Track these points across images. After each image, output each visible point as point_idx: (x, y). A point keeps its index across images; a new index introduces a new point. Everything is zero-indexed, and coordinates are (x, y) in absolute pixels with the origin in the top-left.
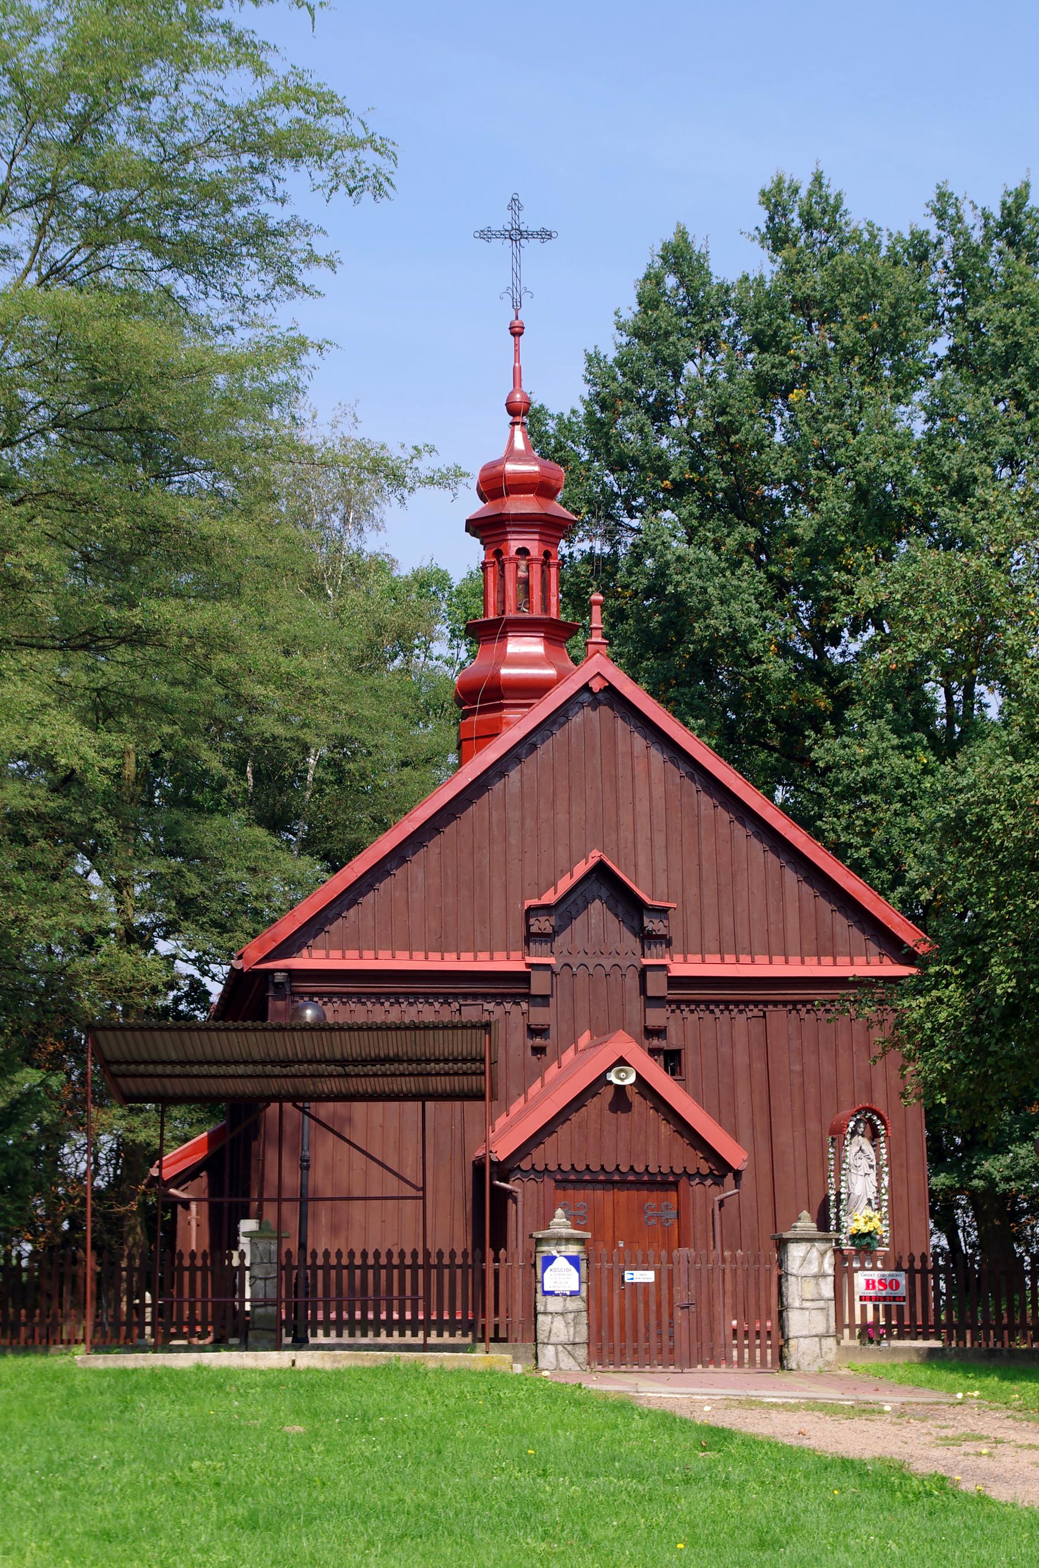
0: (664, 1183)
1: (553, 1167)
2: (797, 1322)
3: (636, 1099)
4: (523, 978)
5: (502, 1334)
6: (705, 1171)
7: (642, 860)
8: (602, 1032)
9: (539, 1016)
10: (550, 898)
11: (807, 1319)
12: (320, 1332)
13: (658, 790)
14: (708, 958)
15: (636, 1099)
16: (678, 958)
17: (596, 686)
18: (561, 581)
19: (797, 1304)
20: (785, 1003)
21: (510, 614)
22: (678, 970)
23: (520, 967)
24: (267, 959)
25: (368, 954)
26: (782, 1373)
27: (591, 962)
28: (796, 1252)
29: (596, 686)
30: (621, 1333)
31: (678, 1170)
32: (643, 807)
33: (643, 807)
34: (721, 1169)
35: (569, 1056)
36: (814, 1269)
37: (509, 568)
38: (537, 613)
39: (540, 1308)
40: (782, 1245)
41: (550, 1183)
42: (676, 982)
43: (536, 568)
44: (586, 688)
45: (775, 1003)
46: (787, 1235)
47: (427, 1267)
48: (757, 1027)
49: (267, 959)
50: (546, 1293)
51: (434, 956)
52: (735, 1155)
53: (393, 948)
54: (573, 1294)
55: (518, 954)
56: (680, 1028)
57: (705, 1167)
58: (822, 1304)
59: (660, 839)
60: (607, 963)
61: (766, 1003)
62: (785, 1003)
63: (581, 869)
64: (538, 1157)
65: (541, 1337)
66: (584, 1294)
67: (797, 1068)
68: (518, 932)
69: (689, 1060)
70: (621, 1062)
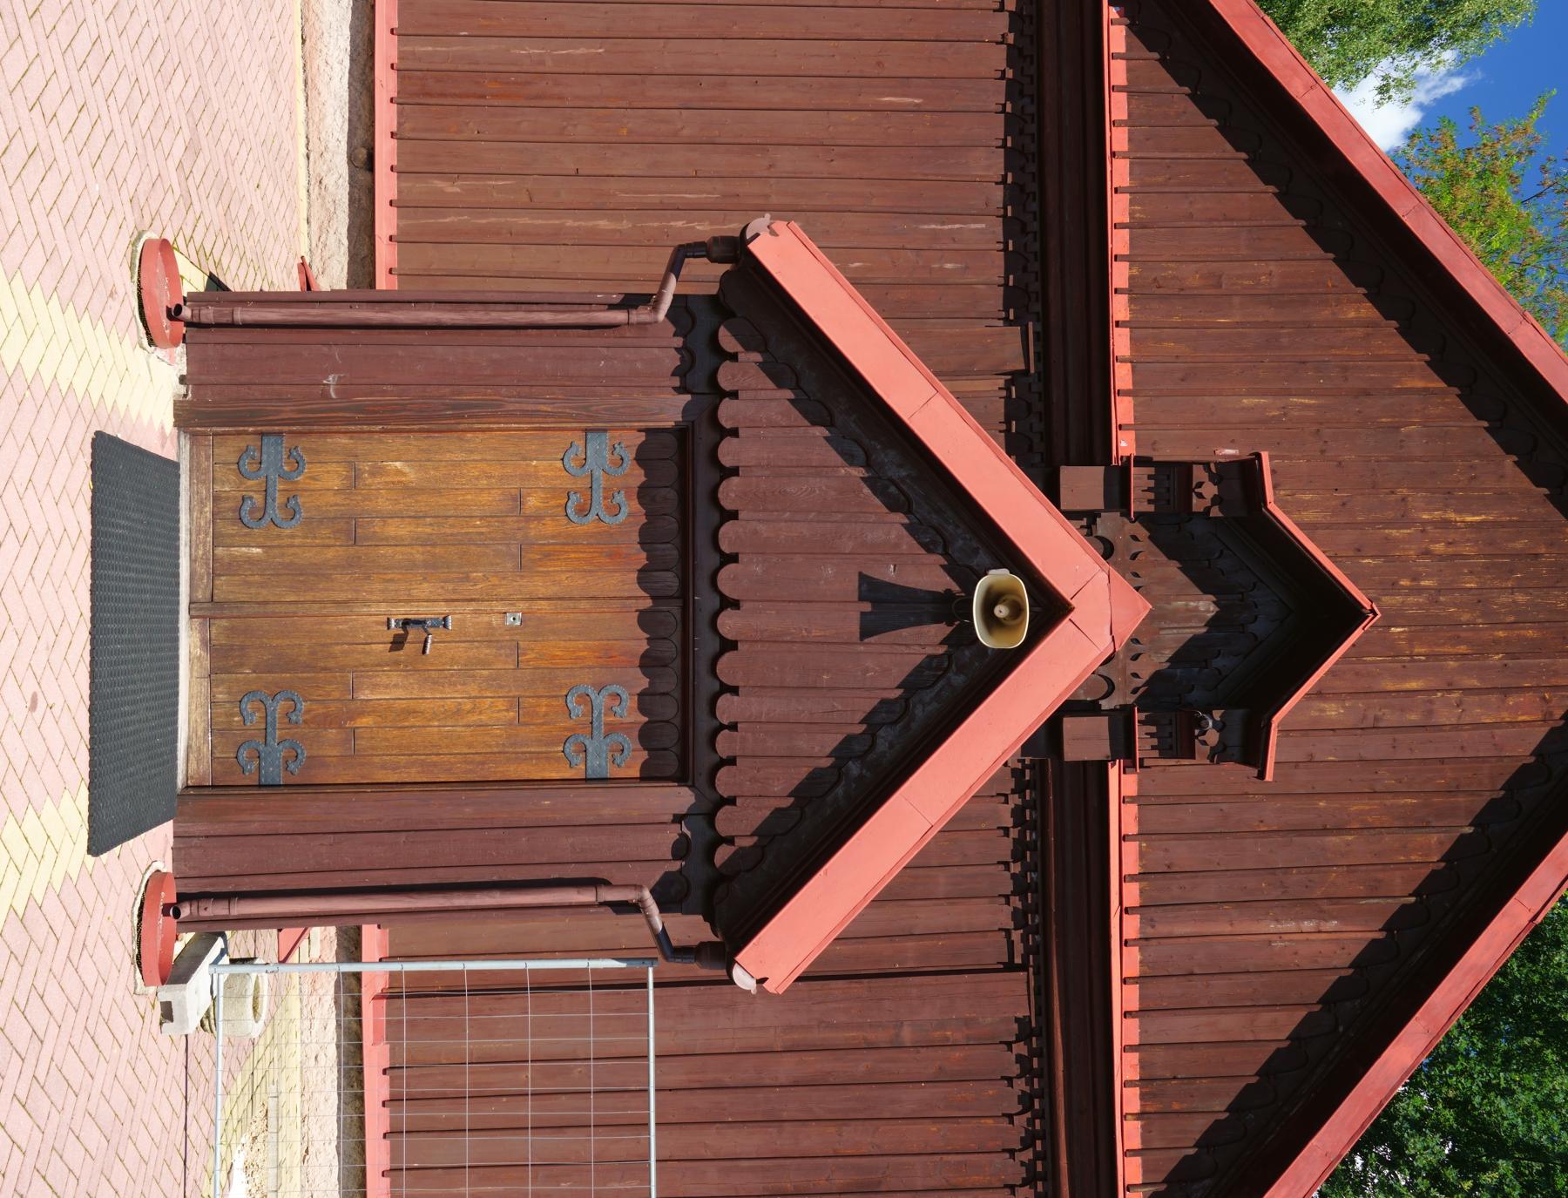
0: (681, 738)
6: (726, 821)
31: (726, 782)
34: (734, 892)
41: (670, 408)
45: (1042, 993)
48: (995, 951)
52: (778, 954)
62: (1044, 1010)
67: (907, 1035)
70: (1050, 608)
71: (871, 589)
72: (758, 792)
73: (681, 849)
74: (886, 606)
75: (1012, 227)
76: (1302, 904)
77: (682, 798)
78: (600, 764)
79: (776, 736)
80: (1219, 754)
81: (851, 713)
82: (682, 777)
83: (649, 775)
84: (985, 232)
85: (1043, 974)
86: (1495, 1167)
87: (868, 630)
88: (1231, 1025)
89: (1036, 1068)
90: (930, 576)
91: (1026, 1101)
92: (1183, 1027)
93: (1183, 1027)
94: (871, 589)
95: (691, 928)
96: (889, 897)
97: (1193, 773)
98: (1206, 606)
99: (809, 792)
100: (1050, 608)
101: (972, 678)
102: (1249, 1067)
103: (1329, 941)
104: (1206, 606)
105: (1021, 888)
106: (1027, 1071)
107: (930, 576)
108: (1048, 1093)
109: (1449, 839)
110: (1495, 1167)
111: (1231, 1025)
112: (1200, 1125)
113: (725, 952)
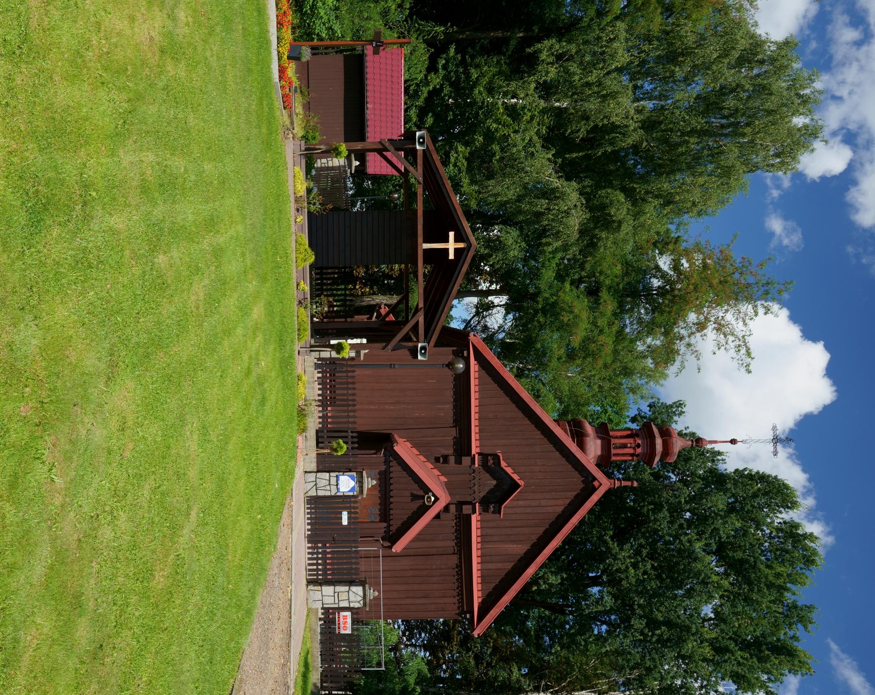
0: (385, 515)
1: (391, 469)
2: (328, 590)
3: (418, 503)
4: (469, 453)
5: (321, 445)
6: (391, 528)
7: (521, 503)
8: (449, 487)
9: (452, 459)
10: (503, 464)
11: (328, 595)
12: (320, 375)
13: (550, 509)
14: (479, 531)
15: (418, 503)
16: (479, 518)
17: (596, 483)
18: (626, 461)
19: (334, 488)
20: (460, 562)
21: (613, 441)
22: (474, 518)
23: (473, 452)
24: (474, 346)
25: (477, 389)
26: (305, 582)
27: (476, 481)
28: (359, 590)
29: (596, 483)
30: (322, 509)
31: (391, 522)
32: (543, 503)
33: (543, 503)
34: (392, 538)
35: (436, 472)
36: (352, 598)
37: (631, 440)
38: (613, 451)
39: (332, 474)
40: (362, 584)
41: (383, 468)
42: (468, 518)
43: (631, 451)
44: (595, 479)
45: (460, 558)
46: (367, 586)
47: (321, 279)
48: (451, 550)
49: (474, 346)
50: (337, 477)
51: (477, 416)
52: (398, 548)
53: (480, 399)
54: (338, 489)
55: (478, 450)
56: (450, 521)
57: (393, 529)
58: (337, 601)
59: (529, 510)
60: (476, 488)
61: (460, 555)
62: (460, 562)
63: (516, 477)
64: (396, 468)
65: (319, 475)
66: (338, 494)
67: (434, 567)
68: (487, 451)
69: (437, 522)
70: (437, 499)
71: (412, 495)
72: (396, 524)
73: (385, 532)
74: (415, 497)
75: (454, 407)
76: (513, 542)
77: (385, 525)
78: (373, 519)
79: (398, 516)
80: (494, 512)
81: (410, 512)
82: (385, 522)
83: (380, 521)
84: (449, 407)
85: (460, 555)
86: (660, 629)
87: (412, 500)
88: (499, 565)
89: (459, 574)
90: (421, 493)
91: (457, 580)
92: (490, 566)
93: (490, 566)
94: (412, 495)
95: (387, 544)
96: (413, 541)
97: (489, 516)
98: (494, 482)
99: (403, 524)
100: (437, 499)
101: (424, 509)
102: (503, 574)
103: (520, 549)
104: (494, 482)
105: (456, 539)
106: (458, 574)
107: (421, 493)
108: (461, 578)
109: (544, 529)
110: (660, 629)
111: (499, 565)
112: (493, 585)
113: (391, 547)
